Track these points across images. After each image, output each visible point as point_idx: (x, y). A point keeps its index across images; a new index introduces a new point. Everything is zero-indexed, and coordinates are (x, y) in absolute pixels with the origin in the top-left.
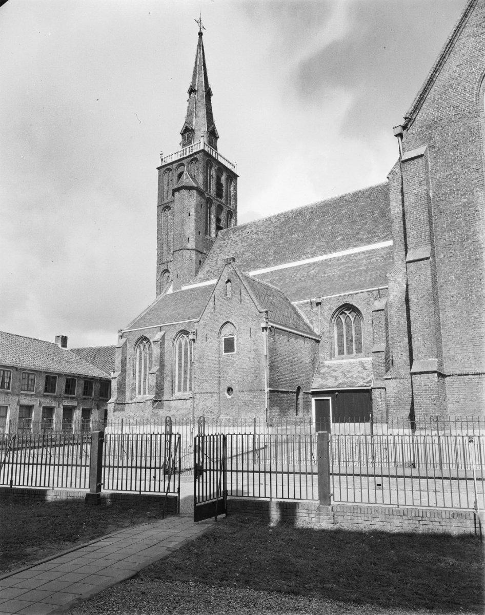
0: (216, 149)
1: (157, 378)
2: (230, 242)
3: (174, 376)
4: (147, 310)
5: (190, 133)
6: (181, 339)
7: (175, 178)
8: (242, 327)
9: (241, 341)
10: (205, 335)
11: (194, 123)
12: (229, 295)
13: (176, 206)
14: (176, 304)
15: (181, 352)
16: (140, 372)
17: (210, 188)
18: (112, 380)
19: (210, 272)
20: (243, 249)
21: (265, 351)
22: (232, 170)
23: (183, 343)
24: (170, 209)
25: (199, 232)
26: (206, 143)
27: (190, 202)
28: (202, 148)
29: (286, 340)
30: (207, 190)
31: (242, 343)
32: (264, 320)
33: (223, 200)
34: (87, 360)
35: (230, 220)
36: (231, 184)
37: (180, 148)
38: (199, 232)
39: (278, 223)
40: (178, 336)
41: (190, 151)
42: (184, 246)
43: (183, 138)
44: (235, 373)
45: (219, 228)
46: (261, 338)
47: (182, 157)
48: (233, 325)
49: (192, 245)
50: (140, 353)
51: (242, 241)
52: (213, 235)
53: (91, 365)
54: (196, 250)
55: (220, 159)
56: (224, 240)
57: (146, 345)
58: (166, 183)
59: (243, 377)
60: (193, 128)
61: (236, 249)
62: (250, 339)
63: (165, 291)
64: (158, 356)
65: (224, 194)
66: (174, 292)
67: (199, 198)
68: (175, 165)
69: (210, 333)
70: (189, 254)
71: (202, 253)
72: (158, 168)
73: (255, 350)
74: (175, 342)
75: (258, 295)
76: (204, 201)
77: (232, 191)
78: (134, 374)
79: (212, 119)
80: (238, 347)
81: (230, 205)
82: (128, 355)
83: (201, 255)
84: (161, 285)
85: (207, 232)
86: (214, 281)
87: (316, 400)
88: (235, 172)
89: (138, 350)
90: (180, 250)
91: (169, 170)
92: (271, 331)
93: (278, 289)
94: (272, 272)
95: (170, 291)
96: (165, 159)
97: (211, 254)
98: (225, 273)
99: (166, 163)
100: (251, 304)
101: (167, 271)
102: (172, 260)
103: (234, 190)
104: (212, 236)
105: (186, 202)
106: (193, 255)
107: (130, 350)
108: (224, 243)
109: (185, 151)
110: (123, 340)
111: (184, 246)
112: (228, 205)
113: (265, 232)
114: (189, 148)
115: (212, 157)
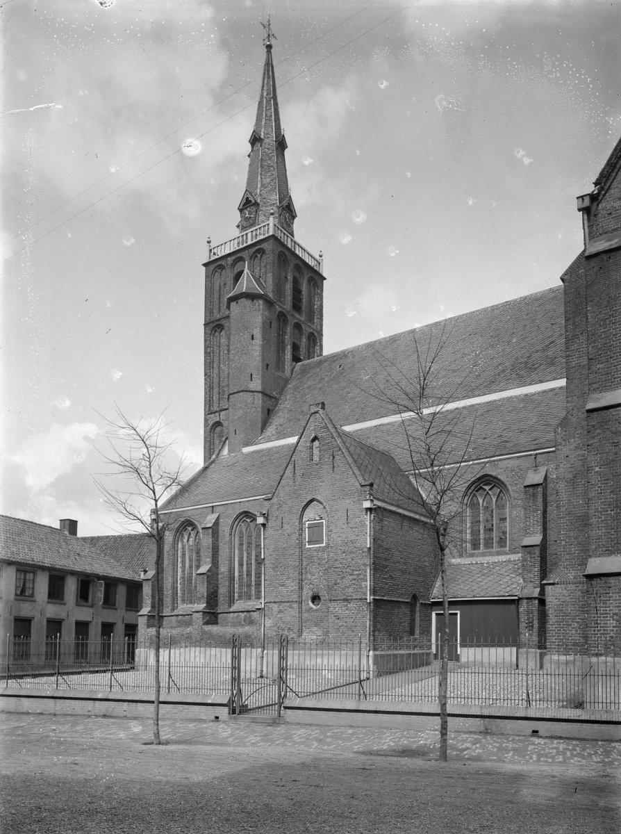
7: (230, 281)
13: (233, 324)
25: (268, 365)
27: (253, 318)
28: (271, 233)
37: (237, 233)
41: (252, 237)
45: (296, 359)
47: (241, 247)
49: (256, 385)
55: (298, 252)
72: (205, 265)
87: (437, 614)
91: (221, 267)
98: (311, 426)
99: (216, 257)
109: (245, 237)
115: (285, 246)
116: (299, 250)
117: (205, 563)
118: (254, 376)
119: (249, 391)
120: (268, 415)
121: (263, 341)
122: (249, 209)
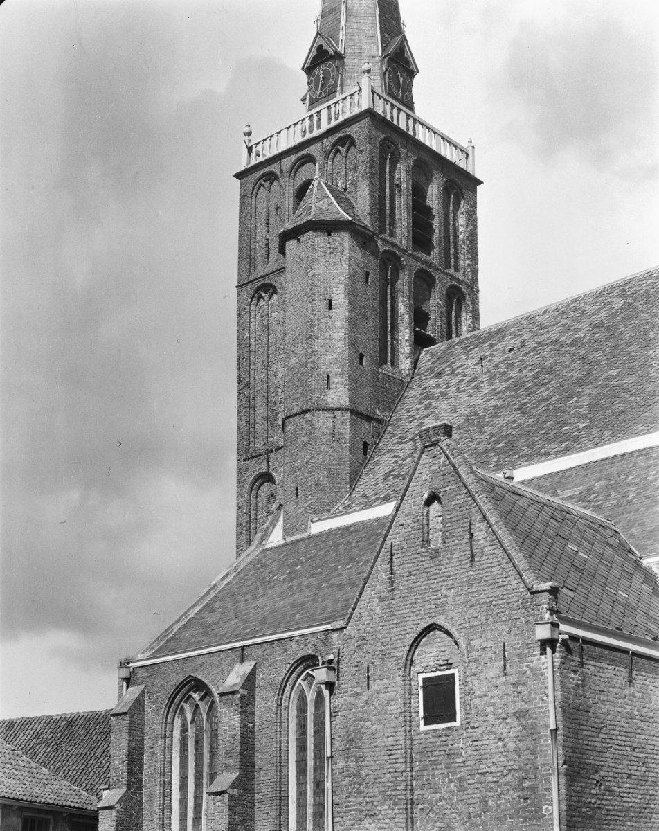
0: (410, 105)
1: (230, 808)
2: (455, 380)
3: (283, 802)
4: (207, 600)
5: (331, 65)
6: (304, 684)
7: (288, 202)
8: (476, 643)
9: (475, 683)
10: (364, 670)
11: (341, 36)
12: (436, 541)
13: (290, 284)
14: (290, 578)
15: (305, 726)
16: (183, 788)
17: (392, 224)
18: (103, 816)
19: (396, 476)
20: (497, 401)
21: (551, 718)
22: (462, 165)
23: (311, 697)
24: (275, 292)
26: (379, 90)
27: (331, 268)
28: (364, 107)
29: (620, 680)
30: (382, 230)
31: (478, 693)
32: (547, 616)
33: (435, 257)
34: (33, 756)
35: (458, 316)
36: (457, 206)
37: (302, 111)
38: (362, 356)
39: (604, 314)
40: (295, 675)
41: (329, 119)
42: (313, 400)
43: (309, 82)
44: (460, 788)
45: (421, 341)
46: (538, 674)
47: (308, 136)
48: (450, 635)
49: (338, 395)
50: (184, 730)
51: (492, 377)
52: (405, 364)
53: (44, 770)
54: (354, 412)
55: (423, 136)
56: (439, 375)
57: (201, 704)
58: (262, 216)
59: (484, 801)
60: (341, 50)
61: (474, 401)
62: (503, 679)
63: (262, 539)
64: (234, 737)
65: (436, 238)
66: (289, 539)
67: (359, 254)
68: (287, 162)
69: (378, 662)
70: (330, 423)
71: (369, 419)
72: (238, 176)
73: (519, 715)
74: (287, 692)
75: (526, 540)
76: (373, 263)
77: (461, 229)
78: (166, 796)
79: (398, 18)
80: (467, 705)
81: (457, 269)
82: (146, 740)
83: (366, 426)
84: (249, 523)
85: (385, 353)
86: (387, 509)
88: (470, 170)
89: (178, 723)
90: (304, 412)
91: (271, 177)
92: (568, 650)
93: (599, 517)
94: (585, 467)
95: (276, 537)
96: (260, 147)
97: (398, 420)
98: (423, 474)
99: (261, 159)
100: (505, 572)
101: (266, 477)
102: (281, 443)
103: (468, 225)
104: (402, 367)
105: (319, 269)
106: (344, 426)
107: (153, 718)
108: (438, 386)
109: (315, 119)
110: (134, 692)
111: (313, 400)
112: (451, 271)
113: (562, 346)
114: (329, 107)
115: (396, 129)
116: (452, 151)
117: (228, 768)
118: (334, 380)
119: (324, 410)
120: (365, 453)
121: (350, 312)
122: (322, 67)
